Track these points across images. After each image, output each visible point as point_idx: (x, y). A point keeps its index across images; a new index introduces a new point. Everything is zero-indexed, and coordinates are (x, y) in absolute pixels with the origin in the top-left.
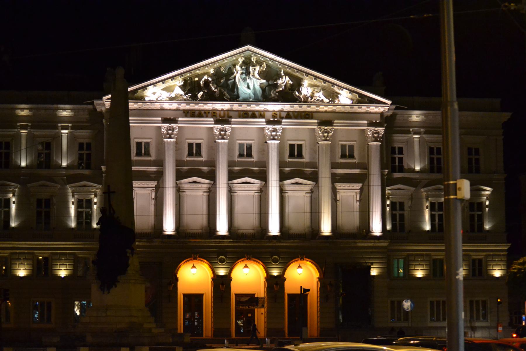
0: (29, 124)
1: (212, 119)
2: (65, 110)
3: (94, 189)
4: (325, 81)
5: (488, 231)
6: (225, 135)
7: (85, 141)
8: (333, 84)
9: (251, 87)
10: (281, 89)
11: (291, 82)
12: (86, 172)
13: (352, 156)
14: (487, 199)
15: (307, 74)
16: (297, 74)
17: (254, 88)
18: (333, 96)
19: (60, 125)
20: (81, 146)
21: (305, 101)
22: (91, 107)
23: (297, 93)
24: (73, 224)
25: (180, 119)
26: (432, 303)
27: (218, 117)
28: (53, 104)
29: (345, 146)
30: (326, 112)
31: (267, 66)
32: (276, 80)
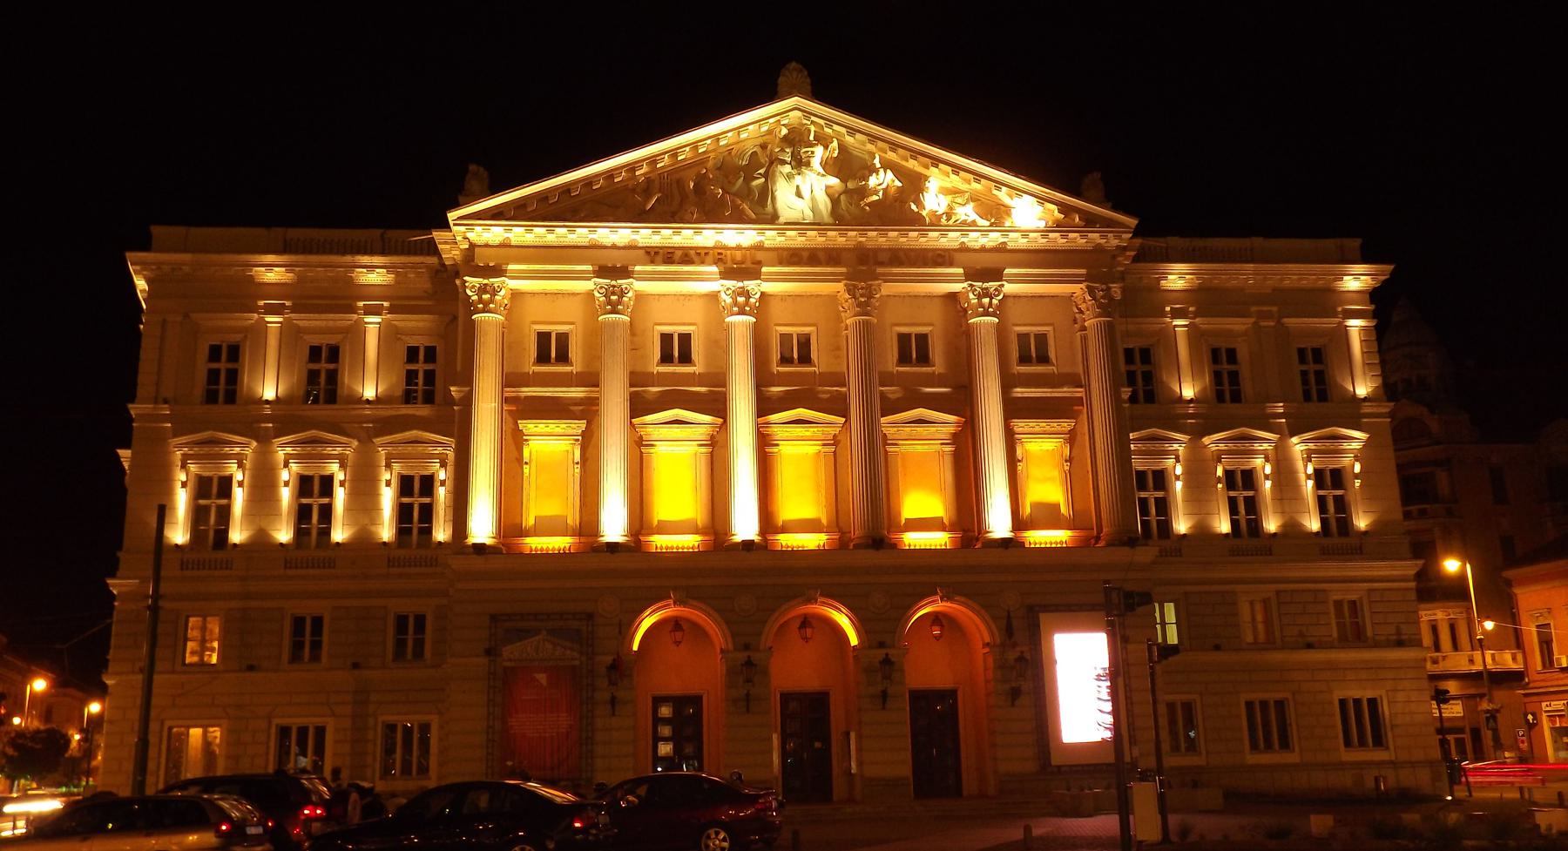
0: (288, 303)
1: (714, 269)
2: (371, 268)
3: (338, 450)
4: (979, 176)
5: (1365, 533)
6: (747, 303)
7: (420, 341)
8: (1000, 184)
9: (805, 192)
10: (875, 198)
11: (898, 184)
12: (423, 411)
13: (1043, 359)
14: (1357, 458)
15: (936, 162)
16: (912, 164)
17: (813, 199)
18: (996, 213)
19: (361, 304)
20: (412, 353)
21: (935, 223)
22: (433, 260)
23: (913, 207)
24: (635, 647)
25: (638, 268)
26: (1249, 705)
27: (729, 264)
28: (344, 254)
29: (1027, 335)
30: (983, 250)
31: (842, 147)
32: (866, 179)
